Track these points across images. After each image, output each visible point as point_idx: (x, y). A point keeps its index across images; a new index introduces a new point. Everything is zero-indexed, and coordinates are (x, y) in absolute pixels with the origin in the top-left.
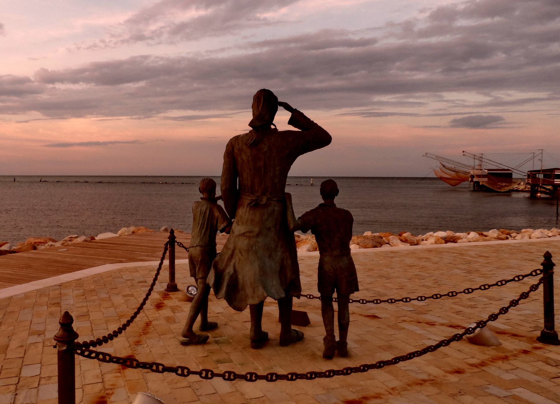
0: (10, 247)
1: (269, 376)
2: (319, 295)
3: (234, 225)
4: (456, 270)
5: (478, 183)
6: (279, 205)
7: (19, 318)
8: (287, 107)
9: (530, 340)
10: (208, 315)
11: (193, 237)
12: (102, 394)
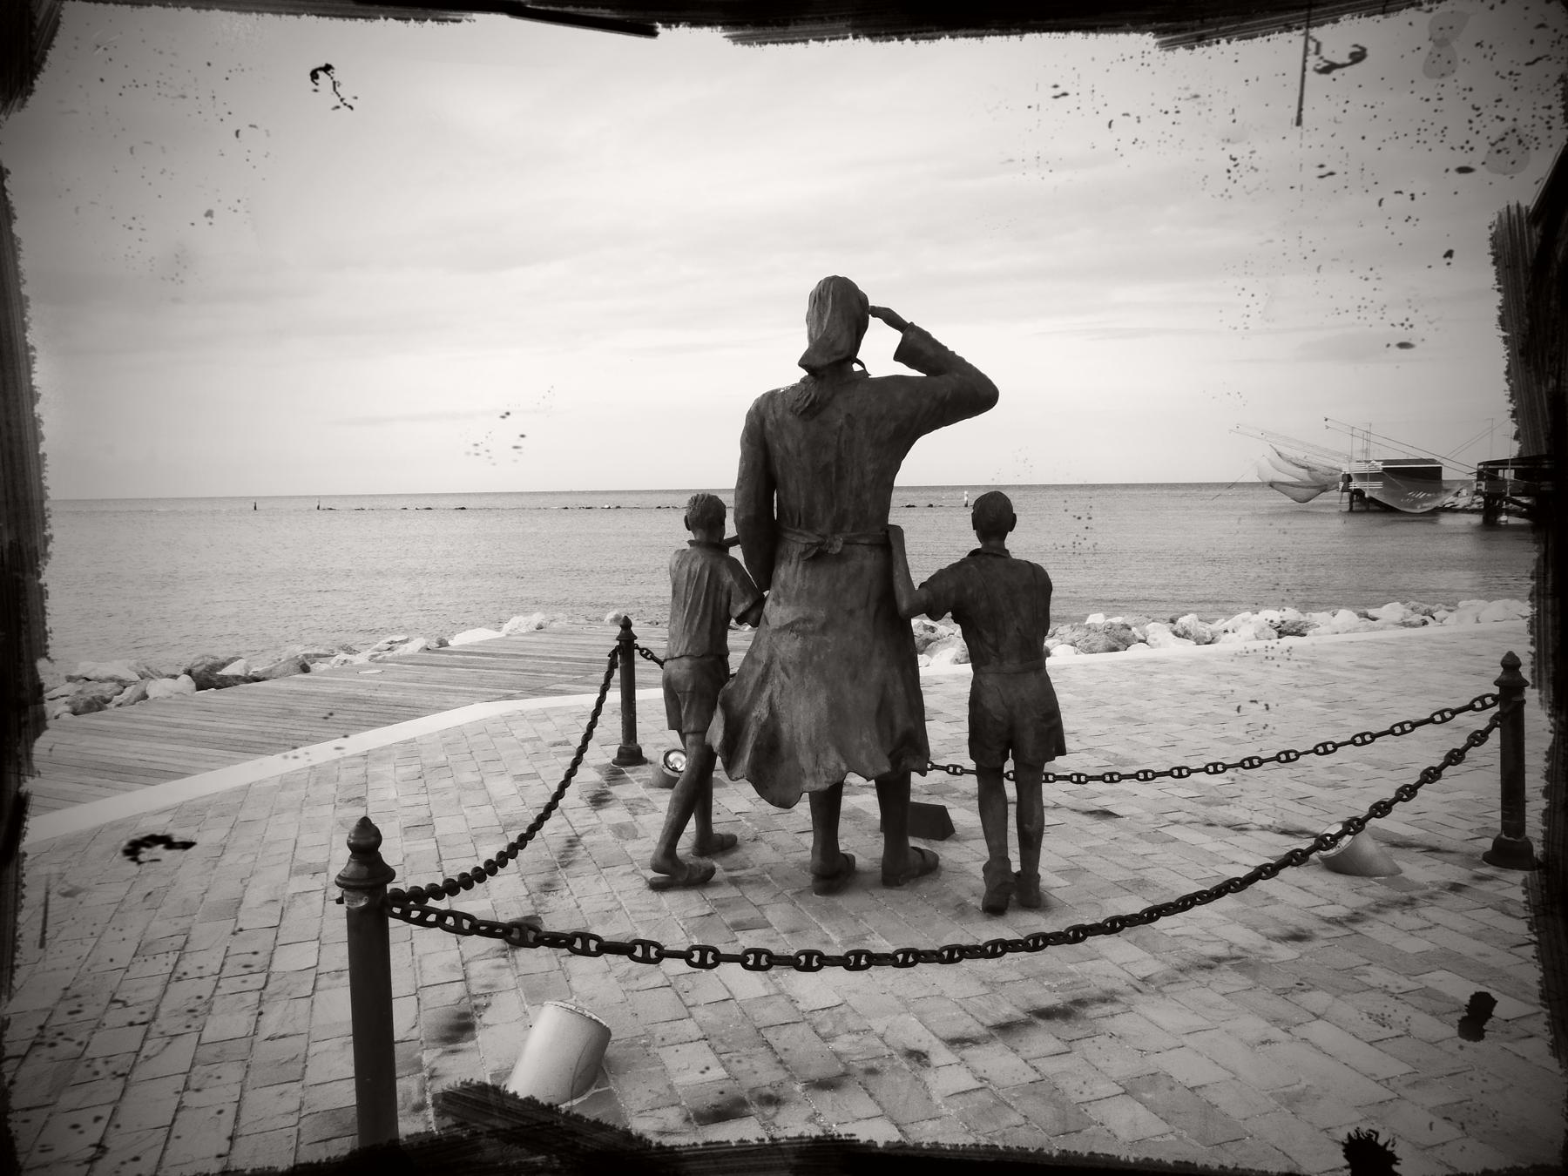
0: (247, 668)
1: (852, 958)
2: (970, 764)
3: (768, 604)
4: (1303, 700)
5: (1359, 493)
6: (873, 554)
7: (268, 834)
8: (892, 319)
9: (1469, 859)
10: (714, 818)
11: (672, 636)
12: (465, 1007)
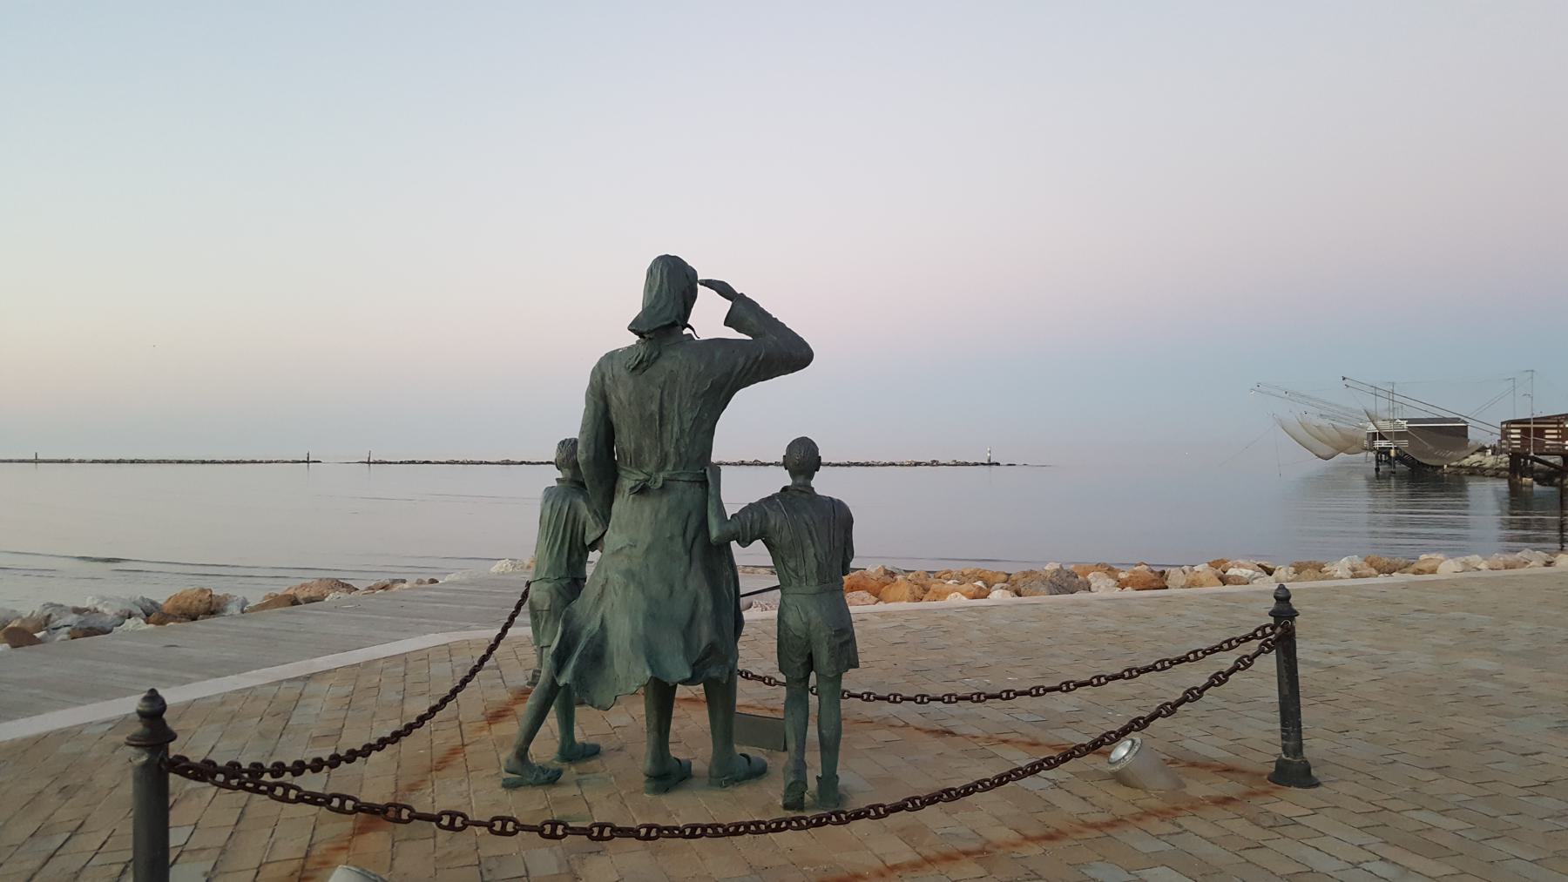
8: (723, 289)
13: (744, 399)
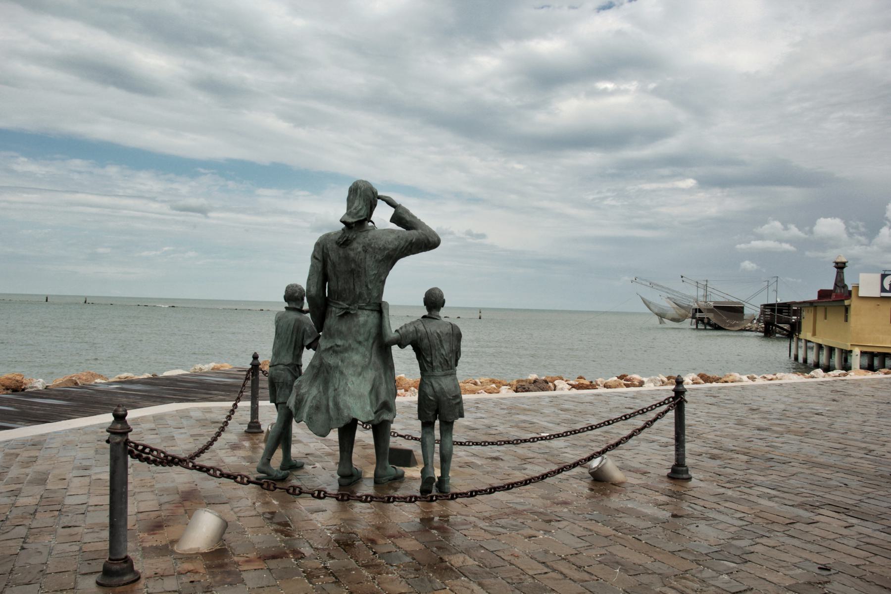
8: (390, 203)
13: (403, 264)
